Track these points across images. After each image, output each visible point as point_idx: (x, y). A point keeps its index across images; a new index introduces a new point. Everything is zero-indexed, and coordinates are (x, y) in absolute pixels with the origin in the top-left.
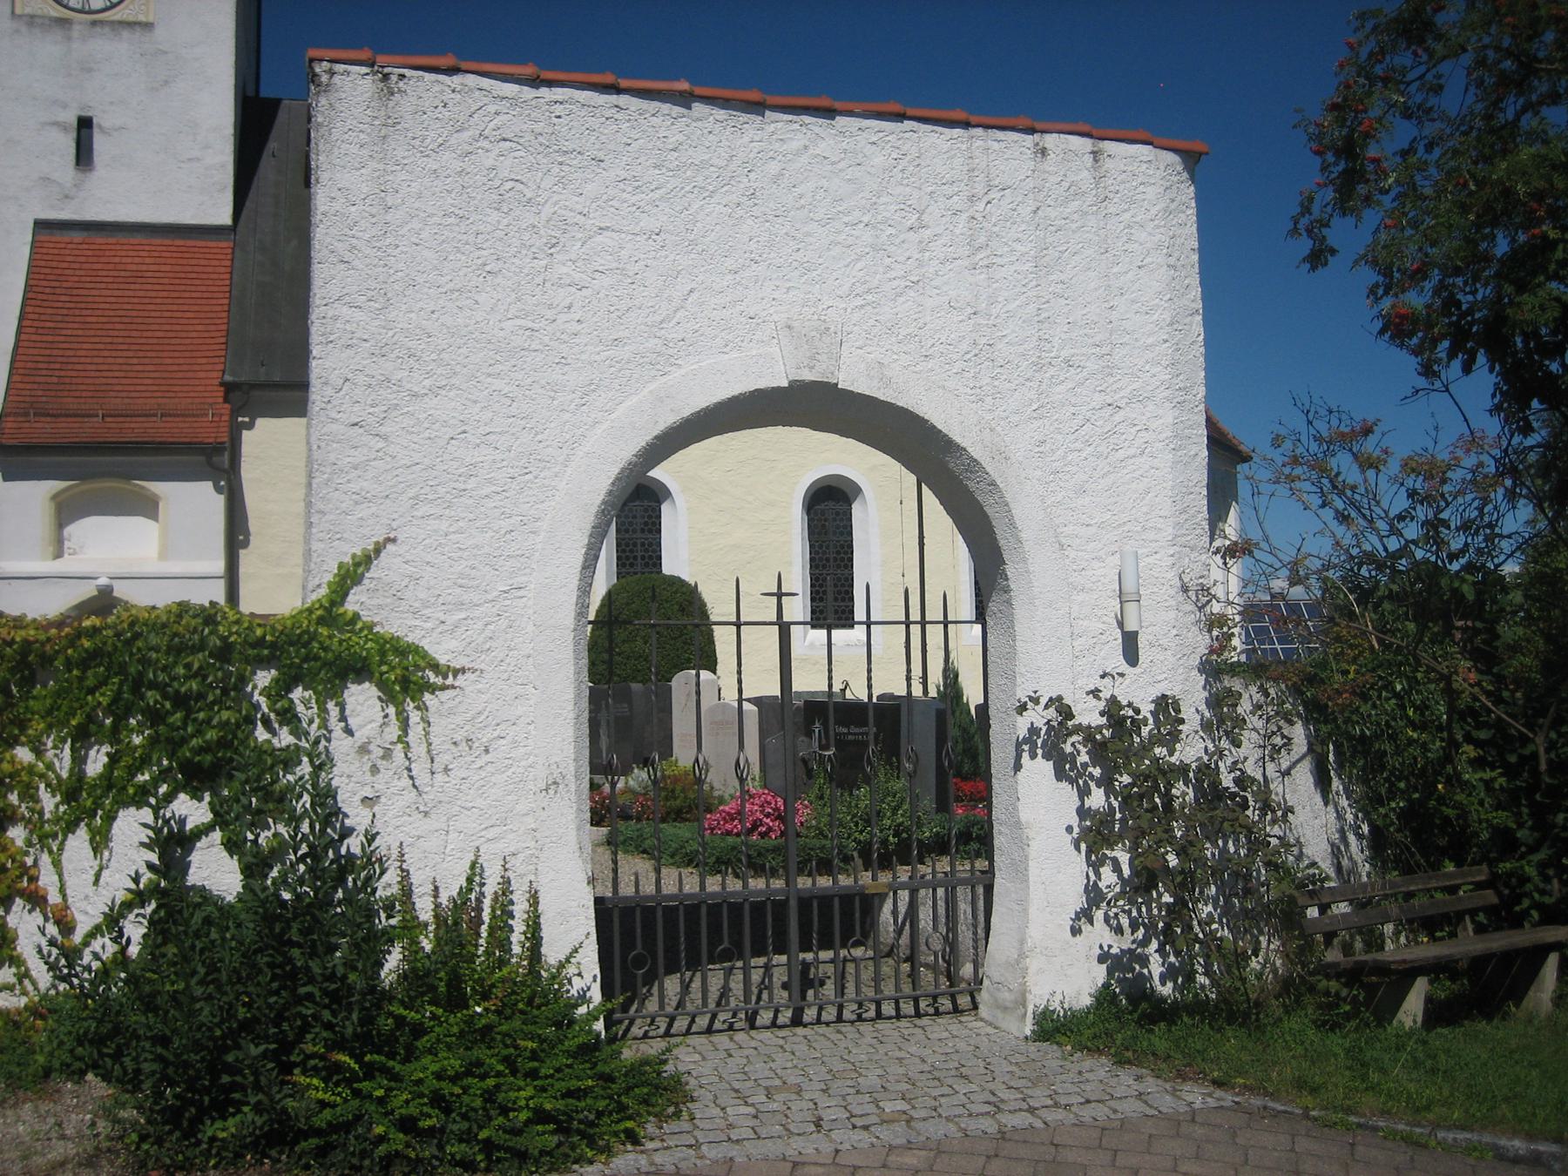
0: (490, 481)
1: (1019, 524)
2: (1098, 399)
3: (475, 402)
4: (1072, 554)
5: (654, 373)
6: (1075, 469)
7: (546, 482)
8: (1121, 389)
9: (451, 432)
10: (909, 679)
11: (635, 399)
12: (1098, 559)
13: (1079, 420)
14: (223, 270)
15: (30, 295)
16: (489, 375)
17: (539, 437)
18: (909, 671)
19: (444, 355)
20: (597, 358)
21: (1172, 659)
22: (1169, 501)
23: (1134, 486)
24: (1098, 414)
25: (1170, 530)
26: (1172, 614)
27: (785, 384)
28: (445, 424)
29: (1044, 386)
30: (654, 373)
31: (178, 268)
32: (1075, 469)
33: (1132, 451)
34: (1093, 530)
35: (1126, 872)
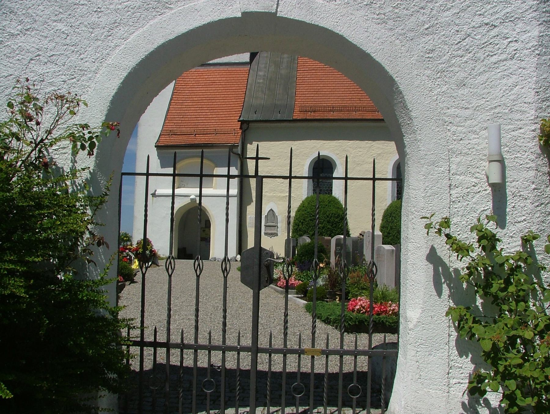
0: (51, 84)
1: (409, 106)
2: (478, 20)
3: (46, 37)
4: (453, 128)
5: (154, 13)
6: (457, 69)
7: (84, 83)
8: (496, 13)
9: (31, 56)
10: (373, 227)
11: (141, 30)
12: (474, 132)
13: (462, 35)
14: (245, 78)
15: (175, 91)
16: (55, 21)
17: (82, 56)
18: (373, 220)
19: (30, 11)
20: (120, 7)
21: (530, 206)
22: (533, 93)
23: (504, 81)
24: (477, 30)
25: (533, 112)
26: (532, 173)
27: (239, 15)
28: (28, 51)
29: (434, 12)
30: (154, 13)
31: (228, 79)
32: (457, 69)
33: (504, 56)
34: (468, 112)
35: (361, 409)
